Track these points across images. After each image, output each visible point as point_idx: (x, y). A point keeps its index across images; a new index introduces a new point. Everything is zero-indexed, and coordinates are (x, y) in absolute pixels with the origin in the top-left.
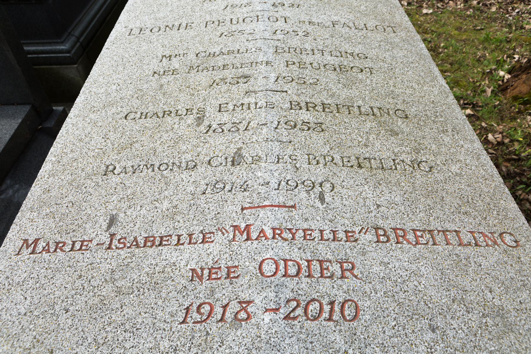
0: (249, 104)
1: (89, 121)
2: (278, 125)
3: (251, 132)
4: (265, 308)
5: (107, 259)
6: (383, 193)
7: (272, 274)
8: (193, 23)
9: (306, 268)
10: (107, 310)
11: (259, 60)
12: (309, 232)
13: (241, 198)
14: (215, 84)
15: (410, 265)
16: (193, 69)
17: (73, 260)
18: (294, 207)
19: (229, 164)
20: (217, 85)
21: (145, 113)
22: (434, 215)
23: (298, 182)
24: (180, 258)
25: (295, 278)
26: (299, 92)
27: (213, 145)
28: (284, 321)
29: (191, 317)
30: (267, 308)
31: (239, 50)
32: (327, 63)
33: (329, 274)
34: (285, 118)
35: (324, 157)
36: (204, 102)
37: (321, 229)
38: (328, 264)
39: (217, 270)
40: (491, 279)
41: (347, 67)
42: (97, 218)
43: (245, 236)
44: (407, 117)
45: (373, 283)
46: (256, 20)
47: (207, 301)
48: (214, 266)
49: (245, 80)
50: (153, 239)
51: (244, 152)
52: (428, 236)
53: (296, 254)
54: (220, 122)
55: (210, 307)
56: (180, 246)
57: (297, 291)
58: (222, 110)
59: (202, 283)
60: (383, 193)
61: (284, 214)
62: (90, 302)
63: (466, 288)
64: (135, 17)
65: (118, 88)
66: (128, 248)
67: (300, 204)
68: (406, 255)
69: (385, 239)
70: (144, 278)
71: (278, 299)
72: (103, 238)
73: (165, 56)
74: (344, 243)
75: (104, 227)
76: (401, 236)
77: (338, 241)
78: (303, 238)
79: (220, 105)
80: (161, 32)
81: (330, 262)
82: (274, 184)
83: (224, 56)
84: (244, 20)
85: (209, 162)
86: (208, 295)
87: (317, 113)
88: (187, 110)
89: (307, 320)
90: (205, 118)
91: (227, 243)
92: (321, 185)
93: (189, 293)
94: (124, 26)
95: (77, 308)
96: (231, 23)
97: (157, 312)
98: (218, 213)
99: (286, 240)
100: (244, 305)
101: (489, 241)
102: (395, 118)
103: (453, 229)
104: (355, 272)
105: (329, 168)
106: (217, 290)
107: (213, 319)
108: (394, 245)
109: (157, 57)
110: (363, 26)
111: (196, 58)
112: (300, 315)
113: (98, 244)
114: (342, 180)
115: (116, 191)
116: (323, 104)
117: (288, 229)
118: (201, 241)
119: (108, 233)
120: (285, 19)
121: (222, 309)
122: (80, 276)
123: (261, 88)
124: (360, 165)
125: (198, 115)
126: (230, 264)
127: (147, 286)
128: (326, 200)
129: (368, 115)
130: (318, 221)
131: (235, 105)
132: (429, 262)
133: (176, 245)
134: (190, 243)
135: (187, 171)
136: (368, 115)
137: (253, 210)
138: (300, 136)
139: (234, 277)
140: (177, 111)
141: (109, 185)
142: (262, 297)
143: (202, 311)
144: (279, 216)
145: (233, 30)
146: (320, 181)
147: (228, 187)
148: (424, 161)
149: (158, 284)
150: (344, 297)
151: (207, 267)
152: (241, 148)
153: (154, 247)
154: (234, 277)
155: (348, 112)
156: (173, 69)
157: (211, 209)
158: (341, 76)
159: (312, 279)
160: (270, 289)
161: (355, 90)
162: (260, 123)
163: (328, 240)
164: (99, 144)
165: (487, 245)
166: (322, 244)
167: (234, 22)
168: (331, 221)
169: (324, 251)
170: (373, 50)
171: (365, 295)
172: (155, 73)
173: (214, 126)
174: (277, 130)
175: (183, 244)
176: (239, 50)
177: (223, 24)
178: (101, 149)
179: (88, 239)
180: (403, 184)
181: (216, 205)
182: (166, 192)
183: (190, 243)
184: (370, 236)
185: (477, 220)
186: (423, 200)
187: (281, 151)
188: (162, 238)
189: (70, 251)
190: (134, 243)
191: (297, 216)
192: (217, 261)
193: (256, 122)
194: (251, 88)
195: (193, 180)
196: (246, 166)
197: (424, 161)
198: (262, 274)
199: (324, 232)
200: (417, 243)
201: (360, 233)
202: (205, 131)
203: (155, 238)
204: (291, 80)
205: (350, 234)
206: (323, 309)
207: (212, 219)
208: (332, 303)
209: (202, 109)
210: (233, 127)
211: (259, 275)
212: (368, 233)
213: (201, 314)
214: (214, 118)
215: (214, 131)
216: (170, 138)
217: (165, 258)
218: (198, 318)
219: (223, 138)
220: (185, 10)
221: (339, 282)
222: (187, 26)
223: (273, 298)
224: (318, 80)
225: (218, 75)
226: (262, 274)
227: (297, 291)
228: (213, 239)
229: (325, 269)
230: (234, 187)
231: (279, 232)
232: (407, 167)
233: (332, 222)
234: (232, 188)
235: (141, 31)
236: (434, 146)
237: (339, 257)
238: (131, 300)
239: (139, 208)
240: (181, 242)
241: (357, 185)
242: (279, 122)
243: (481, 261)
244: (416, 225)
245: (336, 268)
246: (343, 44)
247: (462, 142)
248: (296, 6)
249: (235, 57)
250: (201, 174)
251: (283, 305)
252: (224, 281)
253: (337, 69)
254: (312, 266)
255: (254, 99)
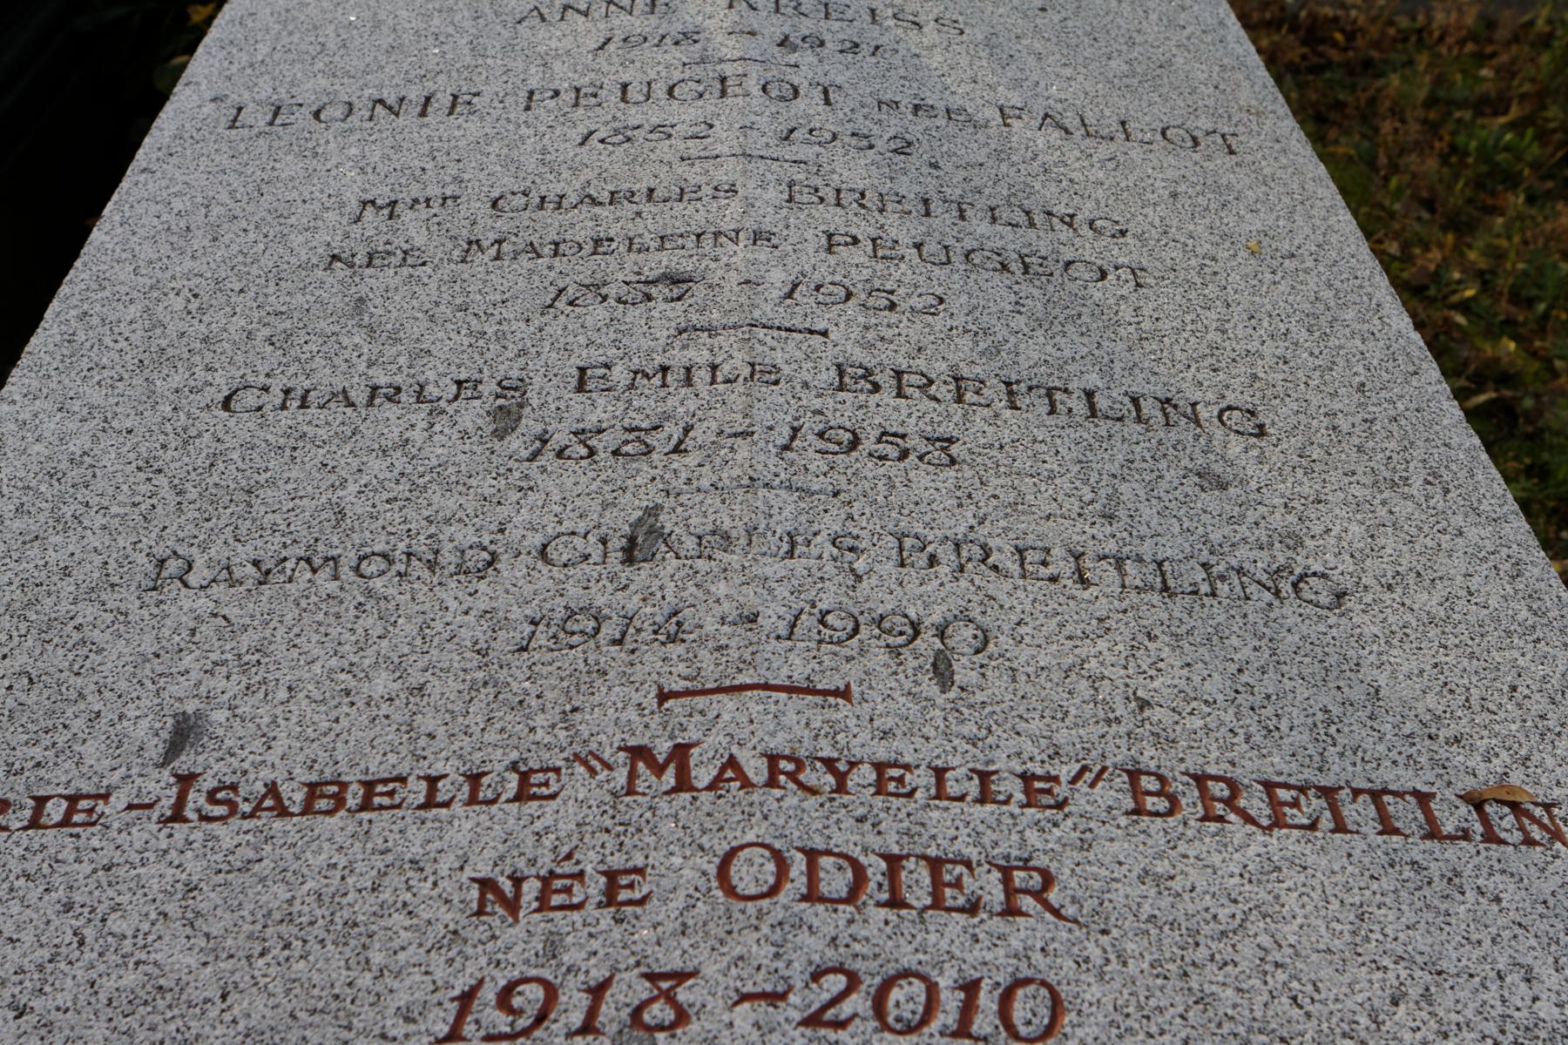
0: (688, 370)
1: (85, 411)
2: (793, 438)
3: (692, 460)
4: (737, 990)
5: (165, 852)
6: (1161, 665)
7: (765, 889)
8: (477, 94)
9: (879, 878)
10: (170, 1007)
11: (727, 225)
12: (895, 772)
13: (663, 665)
14: (564, 298)
15: (1248, 887)
16: (480, 248)
17: (39, 857)
18: (845, 694)
19: (615, 557)
20: (571, 303)
21: (299, 392)
22: (1341, 740)
23: (861, 619)
24: (438, 845)
25: (841, 907)
26: (871, 335)
27: (557, 498)
28: (801, 1029)
29: (477, 1022)
30: (745, 990)
31: (651, 191)
32: (975, 244)
33: (961, 901)
34: (818, 418)
35: (957, 546)
36: (522, 360)
37: (939, 763)
38: (959, 869)
39: (568, 882)
40: (1533, 942)
41: (1050, 262)
42: (125, 723)
43: (669, 778)
44: (1261, 431)
45: (1115, 932)
46: (717, 94)
47: (533, 972)
48: (559, 871)
49: (676, 292)
50: (335, 789)
51: (666, 521)
52: (1318, 803)
53: (846, 838)
54: (581, 426)
55: (546, 990)
56: (435, 811)
57: (847, 946)
58: (590, 385)
59: (517, 920)
60: (1161, 665)
61: (809, 713)
62: (108, 985)
63: (1444, 965)
64: (252, 65)
65: (194, 306)
66: (244, 817)
67: (866, 684)
68: (1237, 856)
69: (1162, 805)
70: (306, 909)
71: (780, 964)
72: (151, 786)
73: (373, 202)
74: (1017, 811)
75: (155, 750)
76: (1220, 800)
77: (995, 802)
78: (872, 790)
79: (582, 370)
80: (354, 120)
81: (968, 864)
82: (773, 617)
83: (597, 210)
84: (670, 91)
85: (543, 552)
86: (537, 955)
87: (934, 404)
88: (459, 383)
89: (882, 1031)
90: (528, 410)
91: (608, 798)
92: (941, 634)
93: (470, 951)
94: (209, 95)
95: (60, 1002)
96: (624, 100)
97: (353, 1008)
98: (575, 710)
99: (813, 791)
100: (665, 985)
101: (1535, 827)
102: (1219, 433)
103: (1409, 786)
104: (1053, 896)
105: (972, 581)
106: (569, 939)
107: (554, 1027)
108: (1192, 823)
109: (342, 205)
110: (1116, 126)
111: (490, 211)
112: (855, 1015)
113: (130, 807)
114: (1014, 618)
115: (195, 639)
116: (956, 379)
117: (821, 760)
118: (511, 794)
119: (166, 773)
120: (826, 92)
121: (585, 995)
122: (68, 907)
123: (733, 319)
124: (1081, 576)
125: (501, 401)
126: (617, 861)
127: (318, 931)
128: (956, 677)
129: (1119, 419)
130: (927, 739)
131: (636, 373)
132: (1316, 882)
133: (420, 807)
134: (473, 800)
135: (462, 577)
136: (1119, 419)
137: (698, 699)
138: (870, 475)
139: (630, 902)
140: (422, 387)
141: (168, 622)
142: (726, 959)
143: (517, 1002)
144: (791, 718)
145: (633, 122)
146: (937, 618)
147: (609, 630)
148: (1315, 574)
149: (355, 925)
150: (1010, 970)
151: (533, 871)
152: (659, 507)
153: (342, 813)
154: (630, 902)
155: (1047, 408)
156: (406, 247)
157: (549, 695)
158: (1025, 289)
159: (903, 912)
160: (756, 935)
161: (1076, 338)
162: (728, 431)
163: (961, 798)
164: (125, 488)
165: (1529, 842)
166: (937, 807)
167: (634, 94)
168: (973, 741)
169: (949, 827)
170: (1149, 210)
171: (1084, 967)
172: (335, 257)
173: (560, 439)
174: (789, 455)
175: (446, 804)
176: (651, 191)
177: (593, 101)
178: (135, 505)
179: (94, 792)
180: (1234, 641)
181: (565, 684)
182: (385, 643)
183: (473, 800)
184: (1115, 793)
185: (1495, 761)
186: (1303, 692)
187: (803, 518)
188: (369, 786)
189: (25, 828)
190: (268, 803)
191: (852, 722)
192: (569, 856)
193: (714, 426)
194: (695, 318)
195: (483, 607)
196: (675, 562)
197: (1315, 574)
198: (730, 891)
199: (948, 775)
200: (1278, 822)
201: (1074, 781)
202: (525, 454)
203: (344, 786)
204: (843, 294)
205: (1038, 785)
206: (938, 1001)
207: (553, 726)
208: (970, 988)
209: (515, 383)
210: (627, 442)
211: (719, 893)
212: (1100, 784)
213: (511, 1011)
214: (556, 409)
215: (560, 454)
216: (396, 472)
217: (381, 847)
218: (502, 1022)
219: (592, 474)
220: (445, 48)
221: (997, 925)
222: (453, 106)
223: (765, 962)
224: (941, 301)
225: (582, 269)
226: (730, 891)
227: (847, 946)
228: (554, 788)
229: (949, 885)
230: (631, 630)
231: (790, 767)
232: (1252, 588)
233: (974, 745)
234: (624, 634)
235: (276, 114)
236: (1355, 528)
237: (996, 851)
238: (257, 973)
239: (282, 694)
240: (440, 798)
241: (1070, 638)
242: (795, 430)
243: (1501, 887)
244: (1277, 764)
245: (991, 887)
246: (1038, 186)
247: (1458, 520)
248: (865, 50)
249: (639, 214)
250: (513, 589)
251: (799, 984)
252: (597, 913)
253: (1013, 267)
254: (903, 874)
255: (706, 352)
